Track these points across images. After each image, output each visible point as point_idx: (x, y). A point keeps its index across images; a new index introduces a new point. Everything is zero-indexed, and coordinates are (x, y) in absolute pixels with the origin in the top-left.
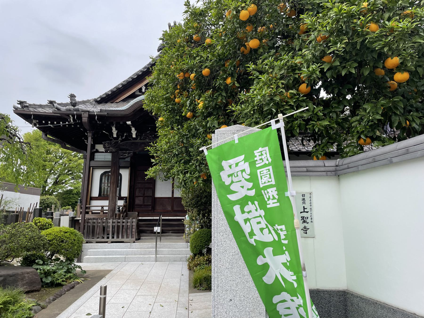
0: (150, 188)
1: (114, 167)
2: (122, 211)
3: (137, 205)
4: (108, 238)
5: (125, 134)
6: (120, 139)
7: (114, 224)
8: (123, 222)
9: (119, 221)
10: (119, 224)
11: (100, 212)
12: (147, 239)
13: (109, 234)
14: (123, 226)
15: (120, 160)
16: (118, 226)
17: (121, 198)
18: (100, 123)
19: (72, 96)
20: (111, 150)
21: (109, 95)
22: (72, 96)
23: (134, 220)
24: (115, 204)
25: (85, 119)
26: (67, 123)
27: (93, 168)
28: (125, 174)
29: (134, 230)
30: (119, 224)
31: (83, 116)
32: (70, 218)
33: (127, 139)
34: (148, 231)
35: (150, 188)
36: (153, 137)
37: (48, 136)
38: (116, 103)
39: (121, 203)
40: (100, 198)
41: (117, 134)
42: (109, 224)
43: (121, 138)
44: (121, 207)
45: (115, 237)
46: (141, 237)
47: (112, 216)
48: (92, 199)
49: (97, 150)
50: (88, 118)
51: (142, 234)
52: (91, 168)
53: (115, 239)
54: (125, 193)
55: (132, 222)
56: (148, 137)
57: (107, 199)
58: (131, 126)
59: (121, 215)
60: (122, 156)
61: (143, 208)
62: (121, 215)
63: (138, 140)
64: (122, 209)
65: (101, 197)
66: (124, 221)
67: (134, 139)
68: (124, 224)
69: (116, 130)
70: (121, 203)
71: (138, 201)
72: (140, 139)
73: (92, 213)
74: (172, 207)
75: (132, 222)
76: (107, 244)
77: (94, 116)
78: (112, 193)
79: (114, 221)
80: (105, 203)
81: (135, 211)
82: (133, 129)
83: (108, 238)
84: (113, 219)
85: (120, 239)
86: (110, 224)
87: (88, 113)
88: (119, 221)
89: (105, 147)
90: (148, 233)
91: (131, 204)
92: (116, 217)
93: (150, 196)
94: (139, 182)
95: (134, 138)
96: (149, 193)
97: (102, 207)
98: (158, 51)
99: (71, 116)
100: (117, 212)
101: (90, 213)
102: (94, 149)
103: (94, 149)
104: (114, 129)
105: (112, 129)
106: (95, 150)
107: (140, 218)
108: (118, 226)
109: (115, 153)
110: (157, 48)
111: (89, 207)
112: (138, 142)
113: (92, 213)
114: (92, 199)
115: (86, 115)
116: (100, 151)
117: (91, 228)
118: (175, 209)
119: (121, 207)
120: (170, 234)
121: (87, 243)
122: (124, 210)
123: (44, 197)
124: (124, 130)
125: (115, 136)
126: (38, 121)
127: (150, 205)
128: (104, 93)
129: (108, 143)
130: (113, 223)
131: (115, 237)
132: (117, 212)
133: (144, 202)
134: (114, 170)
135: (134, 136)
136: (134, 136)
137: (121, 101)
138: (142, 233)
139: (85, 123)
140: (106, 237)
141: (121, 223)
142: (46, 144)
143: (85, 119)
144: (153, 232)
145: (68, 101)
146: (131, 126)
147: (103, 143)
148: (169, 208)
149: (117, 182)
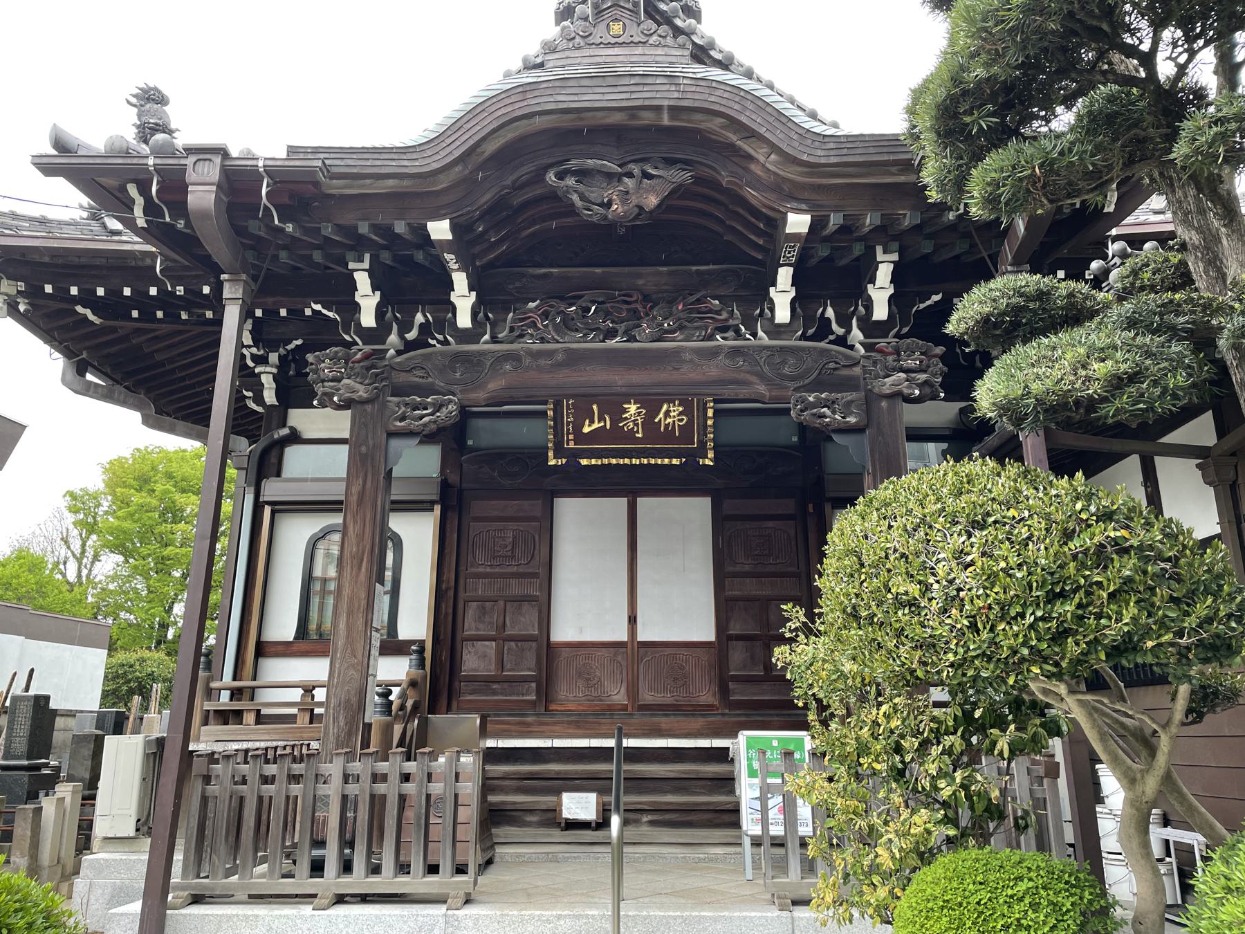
0: (530, 599)
1: (367, 504)
2: (402, 707)
3: (472, 679)
4: (317, 868)
5: (419, 318)
6: (393, 338)
7: (352, 789)
8: (406, 778)
9: (383, 766)
10: (381, 788)
11: (294, 711)
12: (530, 861)
15: (395, 443)
16: (377, 802)
17: (393, 647)
18: (289, 228)
19: (151, 98)
22: (151, 98)
23: (466, 759)
24: (366, 673)
25: (202, 195)
27: (273, 513)
28: (418, 535)
29: (463, 814)
30: (381, 788)
31: (191, 176)
32: (147, 743)
34: (531, 811)
35: (530, 599)
36: (557, 328)
37: (89, 377)
39: (394, 670)
40: (303, 646)
41: (380, 313)
42: (323, 790)
43: (401, 335)
44: (396, 691)
45: (359, 864)
46: (499, 850)
47: (345, 740)
48: (263, 650)
49: (293, 429)
50: (219, 186)
51: (501, 832)
52: (267, 510)
53: (358, 881)
54: (415, 623)
55: (456, 766)
56: (534, 325)
57: (322, 653)
59: (398, 729)
60: (403, 418)
61: (494, 693)
62: (398, 729)
63: (484, 344)
64: (403, 696)
65: (308, 640)
66: (411, 767)
68: (410, 788)
70: (394, 670)
72: (494, 340)
73: (260, 719)
74: (633, 692)
75: (456, 766)
76: (307, 910)
78: (350, 613)
79: (356, 767)
80: (315, 669)
81: (460, 710)
84: (350, 757)
85: (387, 881)
86: (332, 790)
87: (217, 160)
88: (383, 766)
90: (529, 824)
91: (441, 682)
92: (366, 744)
94: (481, 570)
96: (526, 623)
97: (309, 689)
98: (557, 24)
99: (132, 190)
100: (372, 715)
101: (250, 718)
102: (284, 425)
103: (284, 425)
106: (285, 432)
107: (491, 743)
108: (377, 802)
109: (369, 408)
110: (555, 6)
111: (253, 689)
113: (260, 719)
114: (263, 650)
115: (212, 170)
116: (307, 435)
118: (648, 697)
119: (396, 691)
120: (645, 829)
121: (197, 899)
122: (409, 704)
123: (121, 657)
124: (413, 282)
125: (368, 319)
126: (22, 286)
127: (525, 680)
130: (346, 778)
132: (372, 715)
134: (361, 495)
135: (464, 320)
136: (464, 320)
138: (498, 824)
139: (204, 215)
141: (394, 778)
142: (170, 492)
143: (202, 195)
144: (552, 818)
148: (619, 695)
149: (375, 558)
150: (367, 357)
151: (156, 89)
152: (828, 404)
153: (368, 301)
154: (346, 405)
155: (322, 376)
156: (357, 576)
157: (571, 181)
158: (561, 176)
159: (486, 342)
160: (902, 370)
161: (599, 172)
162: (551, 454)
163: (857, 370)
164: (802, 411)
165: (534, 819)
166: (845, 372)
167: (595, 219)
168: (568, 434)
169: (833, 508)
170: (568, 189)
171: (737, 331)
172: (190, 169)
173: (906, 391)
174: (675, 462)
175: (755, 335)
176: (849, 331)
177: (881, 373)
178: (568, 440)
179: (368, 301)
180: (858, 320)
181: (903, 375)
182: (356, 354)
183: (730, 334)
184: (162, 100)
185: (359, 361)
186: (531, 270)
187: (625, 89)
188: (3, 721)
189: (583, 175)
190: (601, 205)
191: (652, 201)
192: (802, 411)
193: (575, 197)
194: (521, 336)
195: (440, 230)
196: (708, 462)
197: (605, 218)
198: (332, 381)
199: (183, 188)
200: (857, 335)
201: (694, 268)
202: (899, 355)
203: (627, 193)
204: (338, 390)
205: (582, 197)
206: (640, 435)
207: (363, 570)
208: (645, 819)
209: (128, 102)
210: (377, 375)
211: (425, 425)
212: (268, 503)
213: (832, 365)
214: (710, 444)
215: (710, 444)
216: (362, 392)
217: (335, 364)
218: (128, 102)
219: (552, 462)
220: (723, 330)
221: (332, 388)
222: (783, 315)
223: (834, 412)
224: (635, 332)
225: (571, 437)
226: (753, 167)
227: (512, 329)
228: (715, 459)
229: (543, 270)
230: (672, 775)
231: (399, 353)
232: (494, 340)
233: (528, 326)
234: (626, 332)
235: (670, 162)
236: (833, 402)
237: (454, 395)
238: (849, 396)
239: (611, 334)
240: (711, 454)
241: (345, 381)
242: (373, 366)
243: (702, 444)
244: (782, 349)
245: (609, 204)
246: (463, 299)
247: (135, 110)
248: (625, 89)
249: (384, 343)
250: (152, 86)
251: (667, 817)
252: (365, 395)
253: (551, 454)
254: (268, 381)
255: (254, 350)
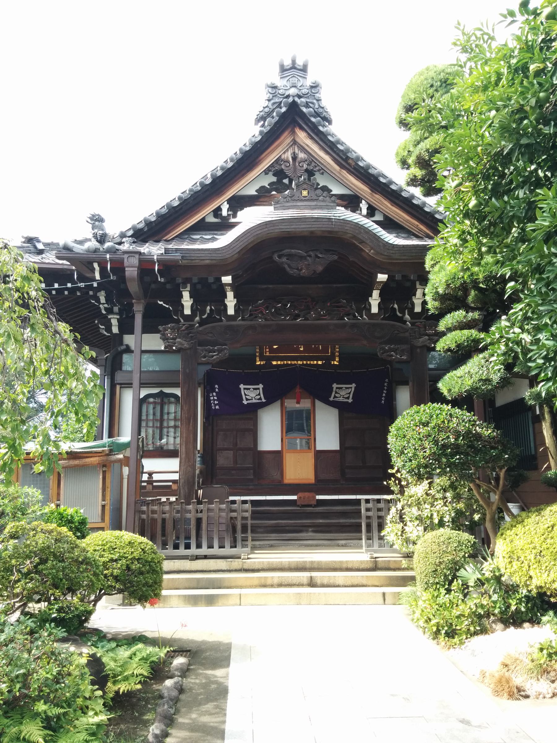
6: (197, 318)
13: (189, 538)
14: (164, 520)
19: (97, 220)
20: (180, 343)
21: (151, 222)
22: (97, 220)
25: (131, 272)
26: (69, 285)
31: (126, 263)
33: (211, 319)
34: (260, 527)
38: (166, 241)
42: (188, 515)
45: (216, 544)
49: (127, 346)
52: (118, 387)
56: (261, 312)
58: (228, 288)
60: (205, 357)
67: (231, 318)
69: (191, 297)
71: (224, 459)
72: (243, 319)
77: (152, 262)
82: (230, 295)
83: (188, 547)
87: (137, 256)
89: (164, 338)
93: (249, 449)
95: (231, 316)
99: (96, 265)
104: (186, 295)
105: (182, 296)
106: (123, 347)
112: (238, 326)
115: (135, 261)
117: (193, 523)
120: (311, 534)
128: (141, 219)
129: (172, 328)
131: (216, 544)
133: (235, 462)
135: (231, 311)
136: (231, 311)
137: (176, 237)
139: (132, 279)
140: (182, 547)
143: (131, 272)
145: (87, 232)
146: (228, 288)
147: (161, 328)
150: (187, 328)
151: (98, 215)
152: (395, 351)
153: (187, 301)
154: (178, 351)
155: (167, 337)
156: (189, 427)
157: (284, 259)
158: (280, 257)
159: (240, 320)
160: (427, 335)
161: (296, 255)
162: (258, 359)
163: (407, 334)
164: (383, 353)
165: (261, 530)
166: (402, 335)
167: (295, 275)
168: (266, 348)
169: (397, 385)
170: (283, 263)
171: (355, 316)
172: (125, 260)
173: (428, 345)
174: (320, 363)
175: (362, 316)
176: (404, 315)
177: (418, 337)
178: (266, 352)
179: (187, 301)
180: (408, 311)
181: (427, 337)
182: (182, 327)
183: (351, 317)
184: (101, 220)
185: (184, 330)
186: (260, 286)
187: (309, 223)
188: (555, 468)
189: (290, 256)
190: (298, 269)
191: (320, 269)
192: (383, 353)
193: (286, 266)
194: (256, 317)
195: (227, 279)
196: (336, 363)
197: (299, 274)
198: (171, 339)
199: (123, 270)
200: (407, 317)
201: (335, 285)
202: (425, 328)
203: (309, 265)
204: (175, 343)
205: (289, 266)
206: (302, 349)
207: (191, 425)
208: (310, 530)
209: (87, 221)
210: (192, 337)
211: (214, 360)
212: (119, 384)
213: (396, 332)
214: (337, 354)
215: (337, 354)
216: (186, 345)
217: (173, 332)
218: (87, 221)
219: (258, 363)
220: (348, 315)
221: (172, 343)
222: (375, 309)
223: (396, 354)
224: (308, 316)
225: (267, 350)
226: (363, 253)
227: (251, 315)
228: (339, 362)
229: (265, 286)
230: (321, 511)
231: (200, 326)
232: (243, 319)
233: (259, 313)
234: (304, 316)
235: (327, 251)
236: (396, 350)
237: (226, 345)
238: (404, 347)
239: (298, 316)
240: (337, 359)
241: (178, 340)
242: (190, 333)
243: (333, 354)
244: (374, 325)
245: (301, 270)
246: (231, 302)
247: (91, 225)
248: (309, 223)
249: (193, 321)
250: (97, 213)
251: (320, 529)
252: (187, 346)
253: (258, 359)
254: (114, 322)
255: (106, 306)
